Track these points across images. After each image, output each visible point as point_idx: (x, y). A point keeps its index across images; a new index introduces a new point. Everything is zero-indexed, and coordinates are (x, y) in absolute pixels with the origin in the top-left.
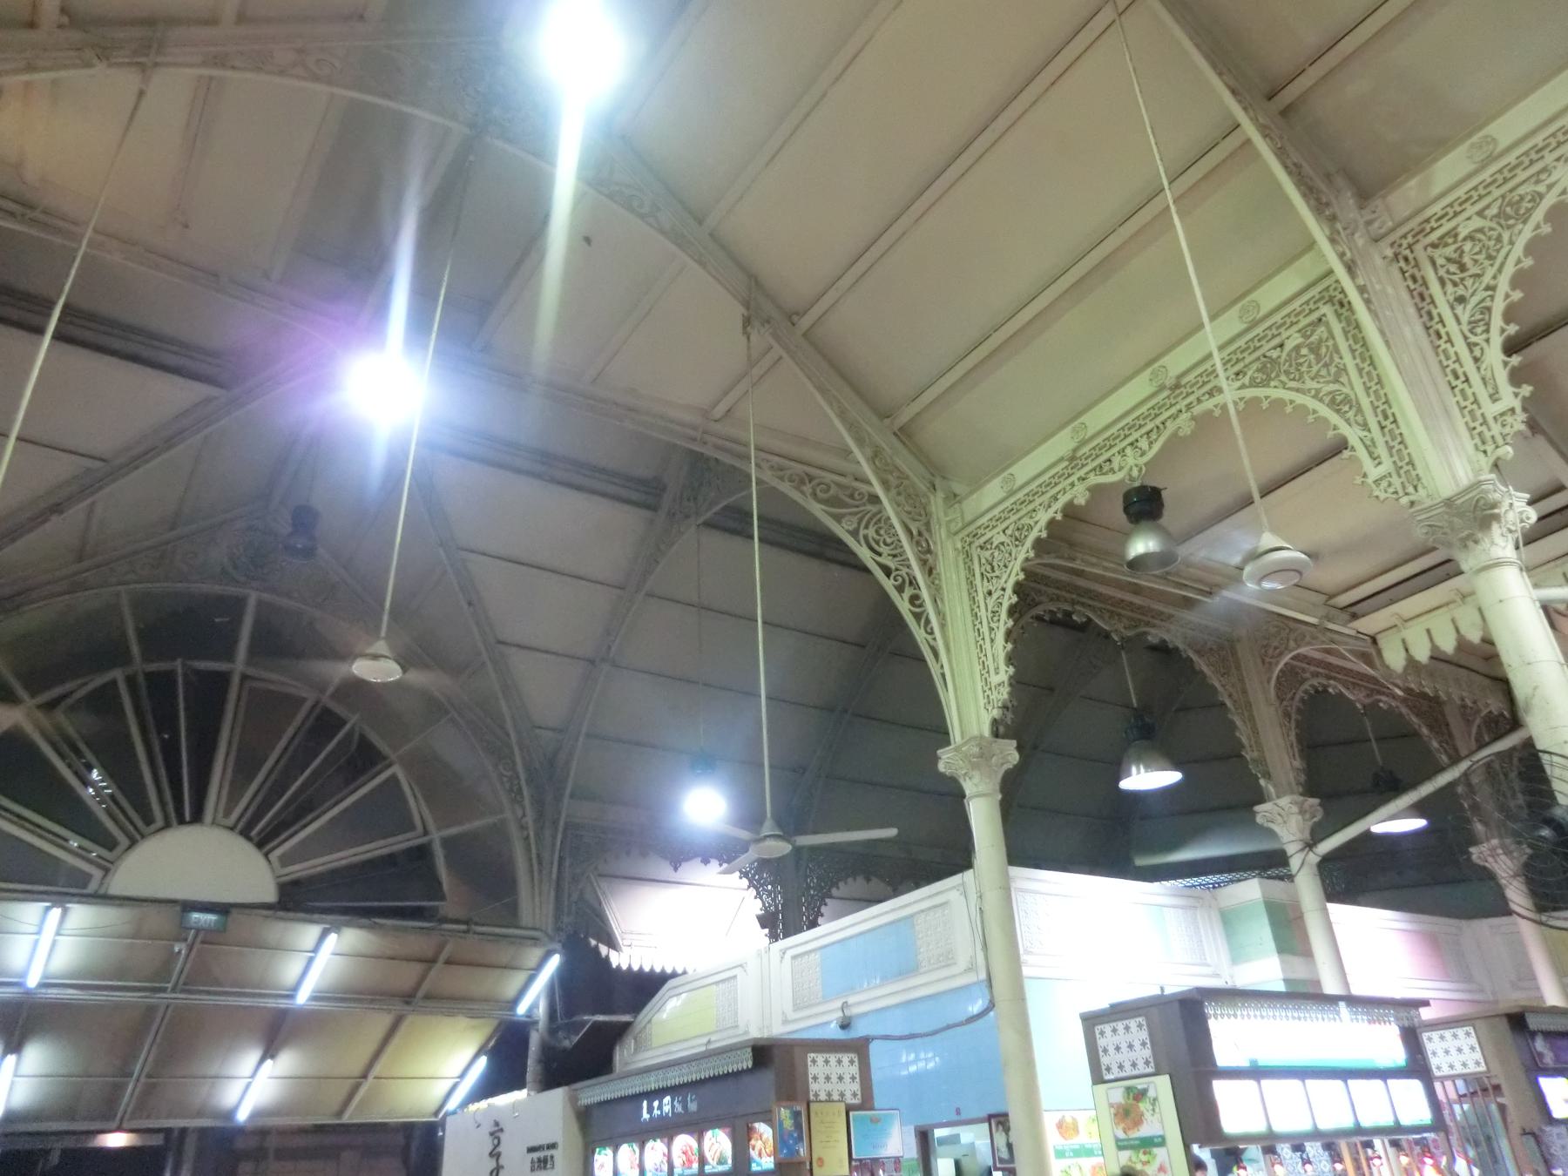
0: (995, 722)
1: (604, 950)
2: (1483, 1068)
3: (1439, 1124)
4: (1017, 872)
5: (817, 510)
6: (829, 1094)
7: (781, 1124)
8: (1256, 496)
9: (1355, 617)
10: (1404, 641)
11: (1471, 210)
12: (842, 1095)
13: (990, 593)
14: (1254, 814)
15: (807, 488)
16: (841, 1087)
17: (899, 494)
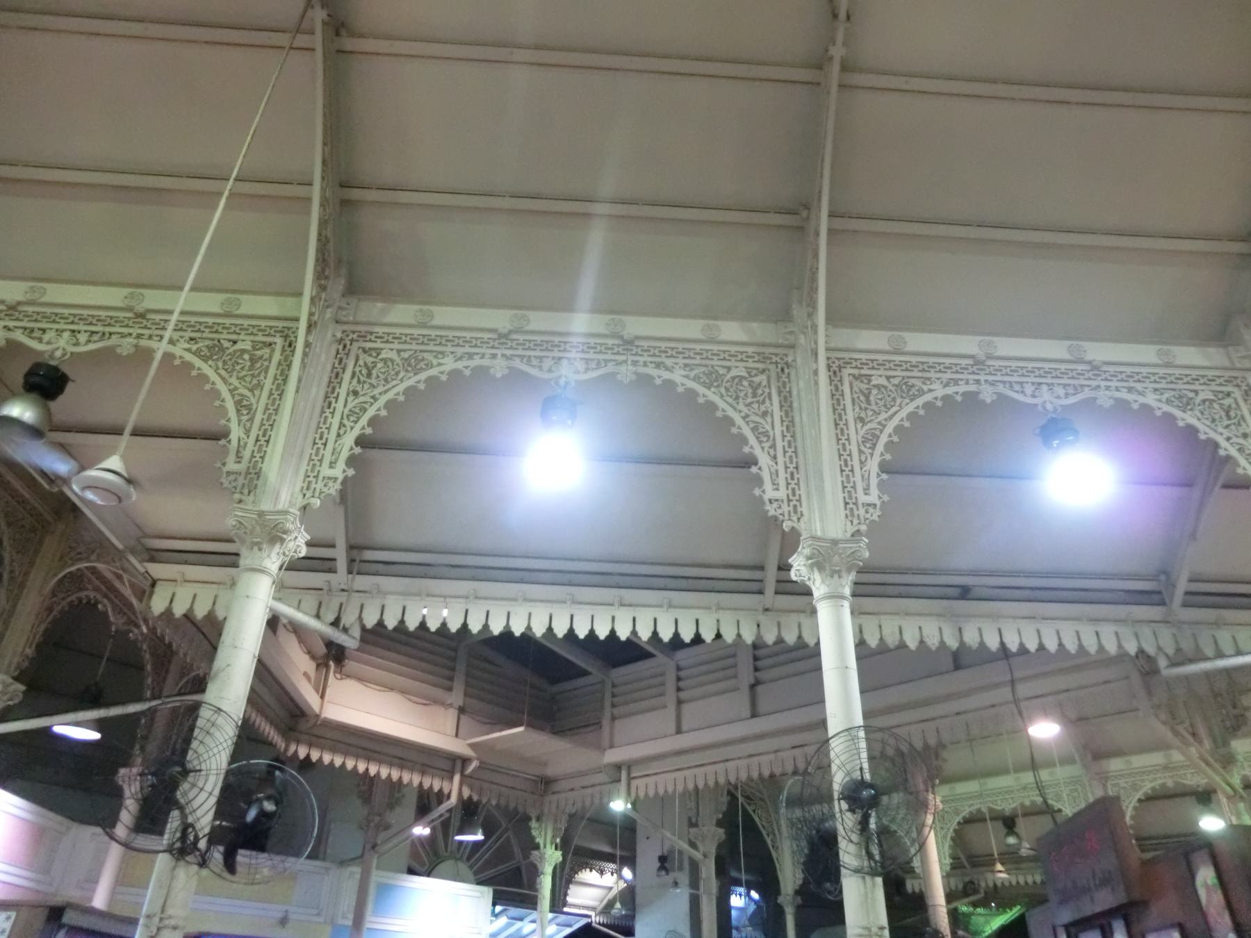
9: (152, 560)
11: (396, 346)
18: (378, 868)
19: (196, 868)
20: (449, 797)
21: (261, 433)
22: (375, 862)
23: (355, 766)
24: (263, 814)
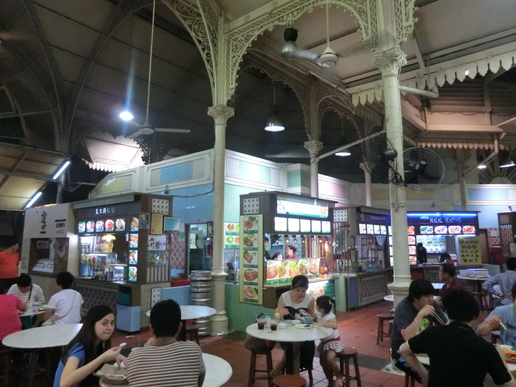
0: (228, 101)
1: (87, 162)
2: (346, 220)
3: (332, 233)
4: (227, 151)
5: (177, 14)
6: (158, 211)
7: (142, 218)
8: (328, 41)
9: (347, 87)
10: (359, 98)
12: (162, 212)
13: (234, 57)
14: (303, 144)
15: (175, 6)
16: (163, 209)
17: (208, 15)
18: (467, 183)
19: (403, 187)
20: (494, 150)
21: (372, 20)
22: (465, 181)
23: (447, 146)
24: (421, 165)
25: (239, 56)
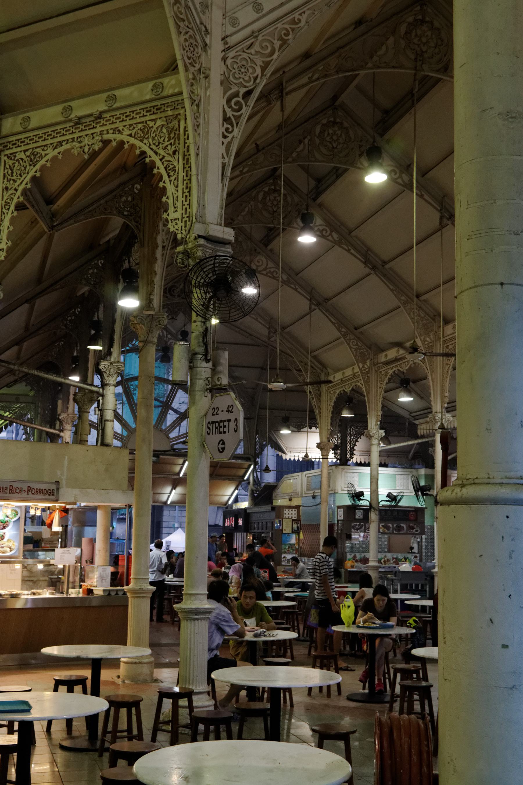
17: (186, 40)
25: (16, 190)
